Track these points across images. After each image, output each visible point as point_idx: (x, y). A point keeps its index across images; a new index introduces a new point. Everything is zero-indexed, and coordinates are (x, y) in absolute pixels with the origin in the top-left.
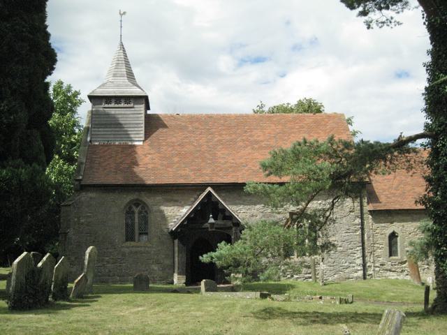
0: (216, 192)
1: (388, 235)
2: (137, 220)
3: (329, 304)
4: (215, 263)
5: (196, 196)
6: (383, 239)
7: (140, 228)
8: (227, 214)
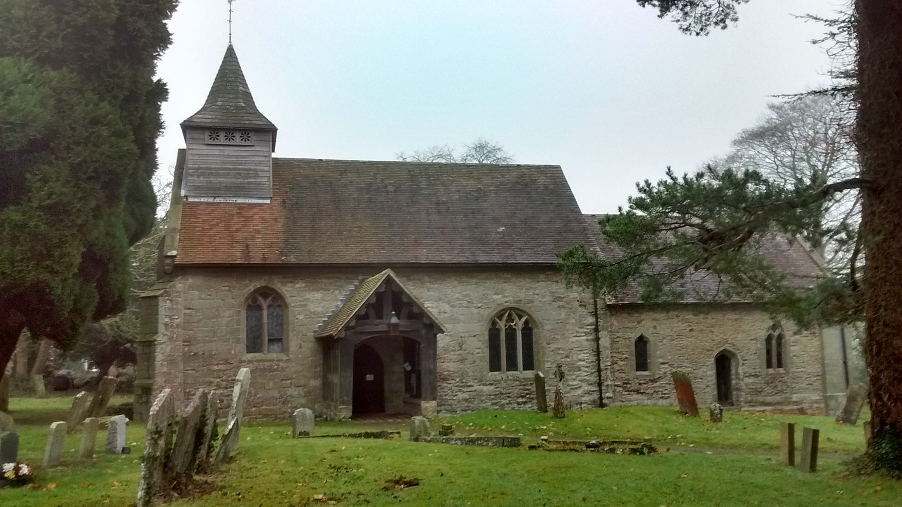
0: (398, 275)
1: (633, 341)
2: (265, 319)
3: (414, 376)
4: (156, 196)
5: (356, 283)
6: (628, 347)
7: (268, 332)
8: (415, 310)
